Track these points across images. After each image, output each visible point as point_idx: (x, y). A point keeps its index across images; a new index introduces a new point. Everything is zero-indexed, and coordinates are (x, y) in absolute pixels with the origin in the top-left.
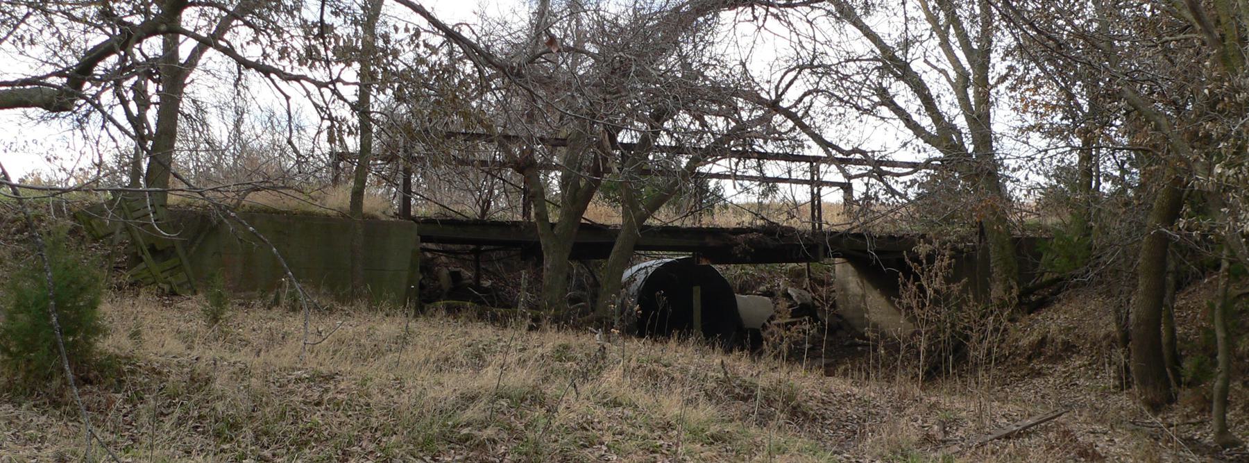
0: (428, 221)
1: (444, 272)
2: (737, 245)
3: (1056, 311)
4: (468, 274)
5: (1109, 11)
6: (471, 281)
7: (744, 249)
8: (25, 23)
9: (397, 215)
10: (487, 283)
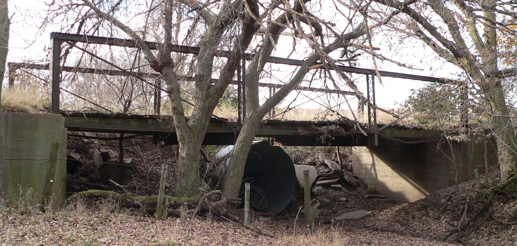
0: (76, 115)
1: (97, 153)
2: (322, 134)
3: (370, 233)
4: (114, 154)
5: (516, 189)
6: (116, 159)
7: (327, 137)
8: (110, 46)
9: (47, 108)
10: (128, 161)
